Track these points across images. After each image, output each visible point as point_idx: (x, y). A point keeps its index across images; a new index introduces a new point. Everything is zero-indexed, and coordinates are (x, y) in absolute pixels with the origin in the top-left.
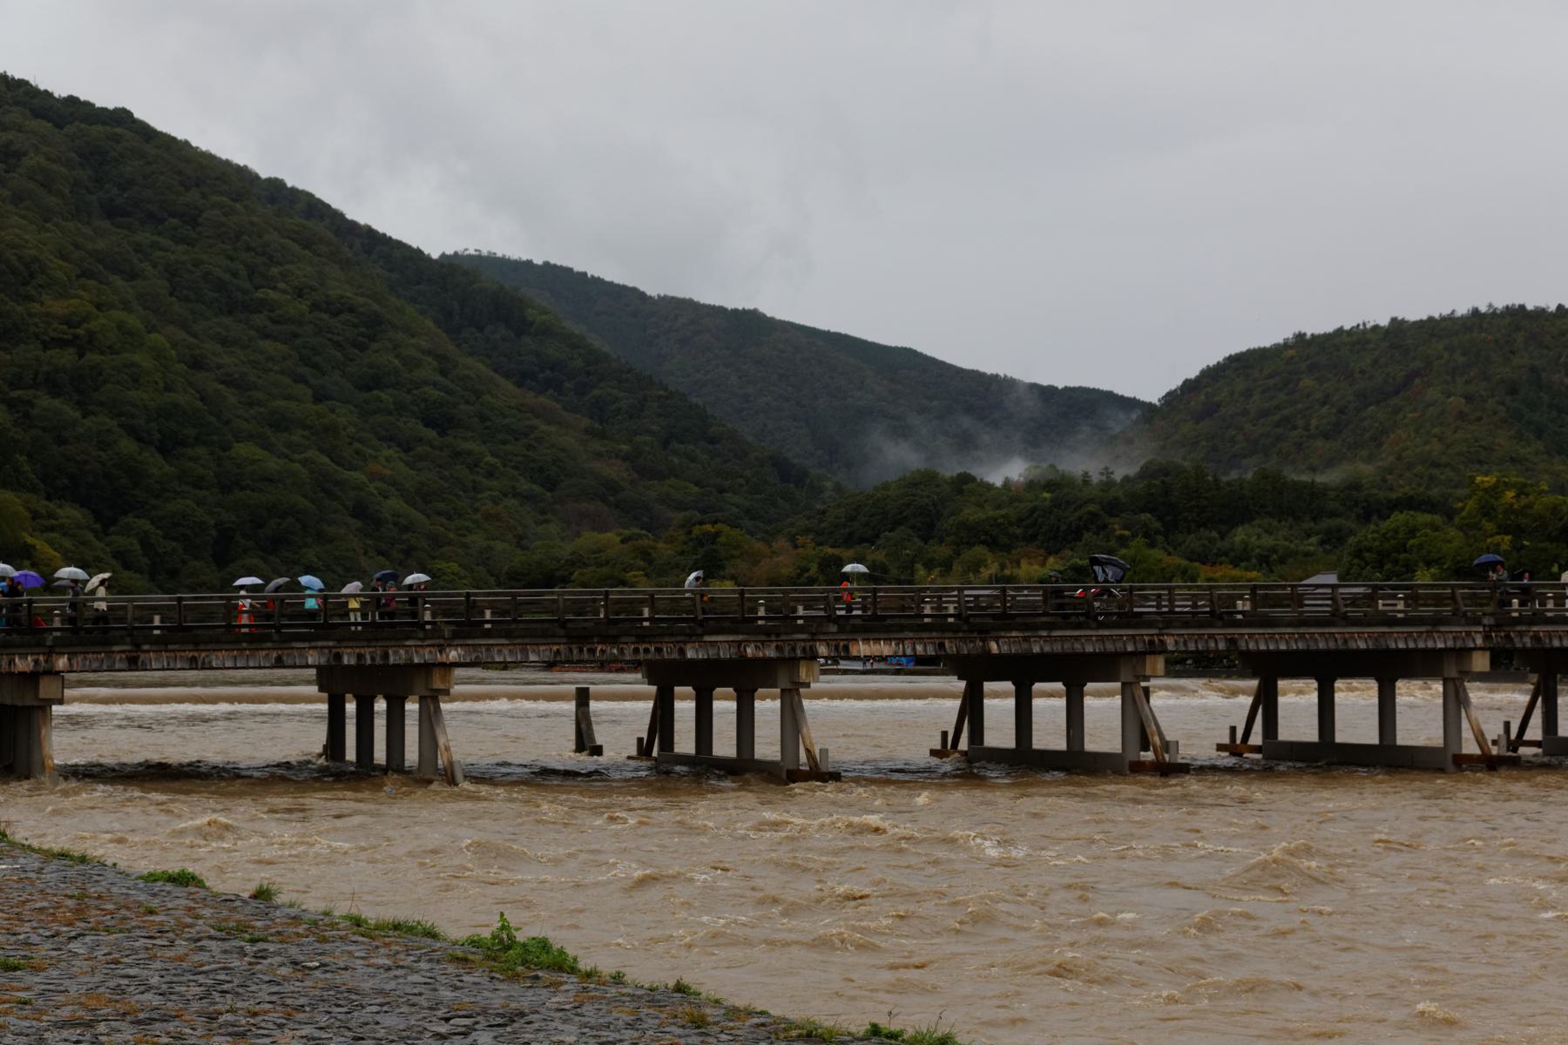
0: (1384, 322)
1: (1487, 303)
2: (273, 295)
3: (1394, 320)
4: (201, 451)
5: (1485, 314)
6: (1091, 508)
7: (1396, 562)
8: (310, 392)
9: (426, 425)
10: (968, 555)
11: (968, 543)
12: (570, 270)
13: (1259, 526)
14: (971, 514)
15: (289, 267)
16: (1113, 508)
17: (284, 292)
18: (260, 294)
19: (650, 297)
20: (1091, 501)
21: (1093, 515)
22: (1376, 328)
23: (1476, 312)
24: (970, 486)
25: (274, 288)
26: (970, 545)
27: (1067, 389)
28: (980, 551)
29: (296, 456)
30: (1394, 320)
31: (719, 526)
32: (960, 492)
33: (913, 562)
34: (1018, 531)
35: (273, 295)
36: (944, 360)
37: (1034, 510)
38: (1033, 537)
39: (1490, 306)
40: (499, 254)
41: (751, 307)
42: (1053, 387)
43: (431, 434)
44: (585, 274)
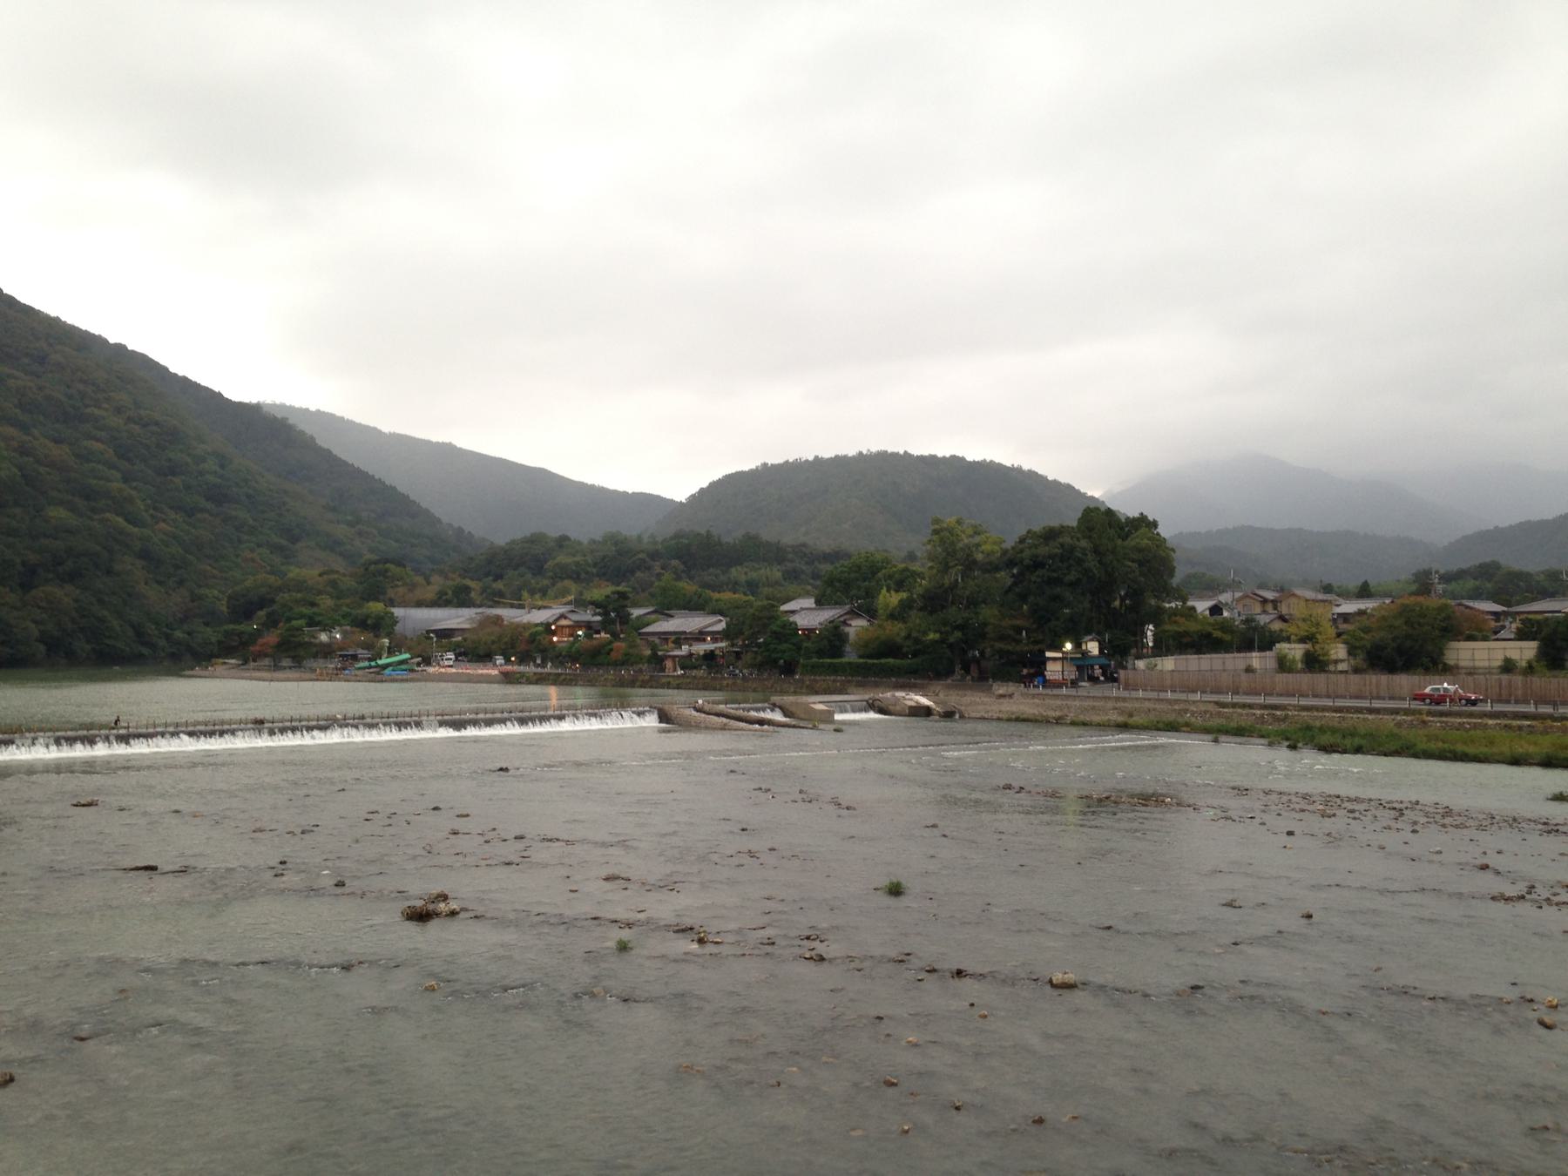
0: (811, 458)
1: (866, 449)
2: (97, 411)
3: (816, 457)
4: (18, 510)
5: (866, 455)
6: (641, 556)
7: (859, 588)
8: (119, 475)
9: (207, 500)
10: (560, 585)
11: (560, 577)
12: (166, 369)
13: (746, 567)
14: (562, 558)
15: (112, 394)
16: (654, 555)
17: (107, 410)
18: (88, 410)
19: (384, 433)
20: (642, 551)
21: (643, 560)
22: (807, 461)
23: (861, 453)
24: (567, 543)
25: (99, 408)
26: (562, 579)
27: (133, 351)
28: (567, 583)
29: (96, 517)
30: (816, 457)
31: (388, 565)
32: (561, 546)
33: (520, 589)
34: (594, 570)
35: (97, 411)
36: (500, 456)
37: (604, 557)
38: (604, 574)
39: (869, 450)
40: (288, 404)
41: (448, 441)
42: (120, 344)
43: (209, 505)
44: (343, 418)
